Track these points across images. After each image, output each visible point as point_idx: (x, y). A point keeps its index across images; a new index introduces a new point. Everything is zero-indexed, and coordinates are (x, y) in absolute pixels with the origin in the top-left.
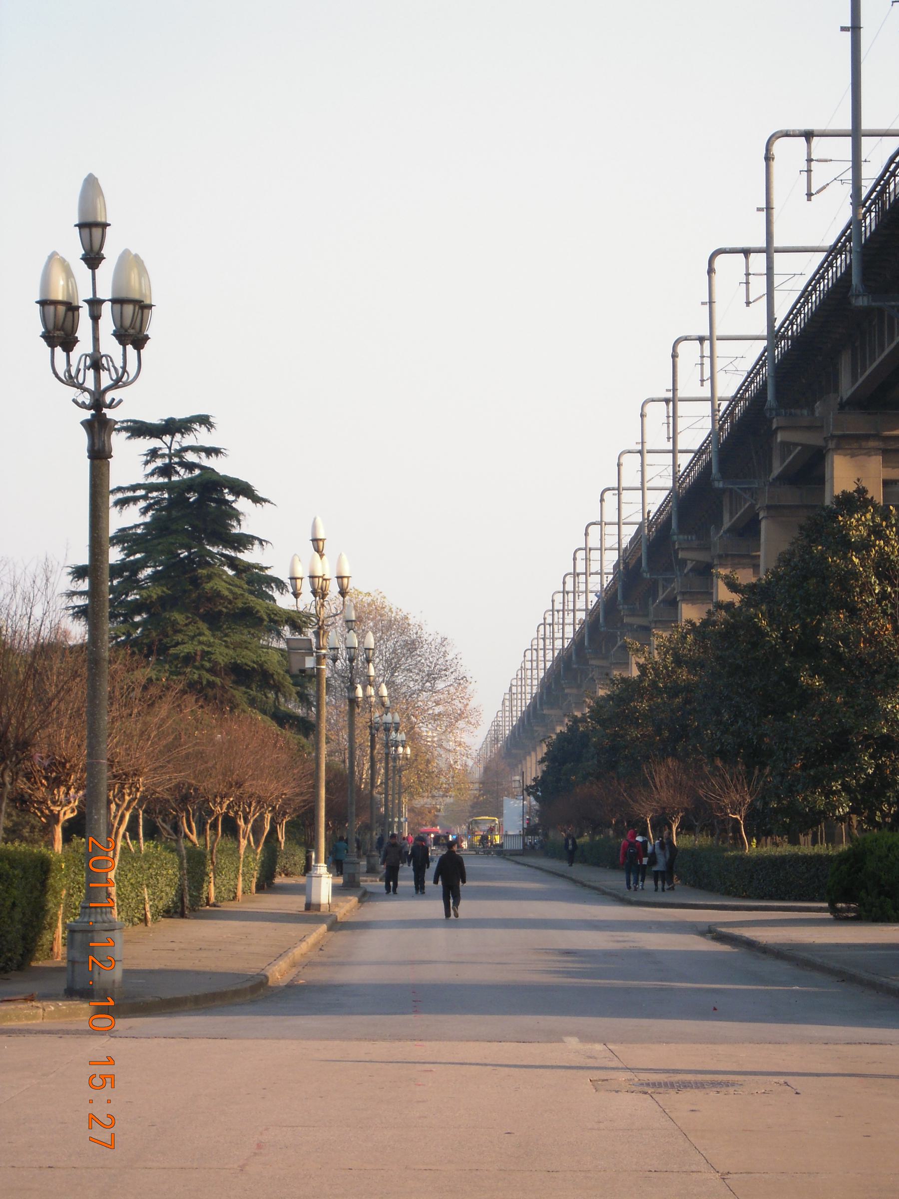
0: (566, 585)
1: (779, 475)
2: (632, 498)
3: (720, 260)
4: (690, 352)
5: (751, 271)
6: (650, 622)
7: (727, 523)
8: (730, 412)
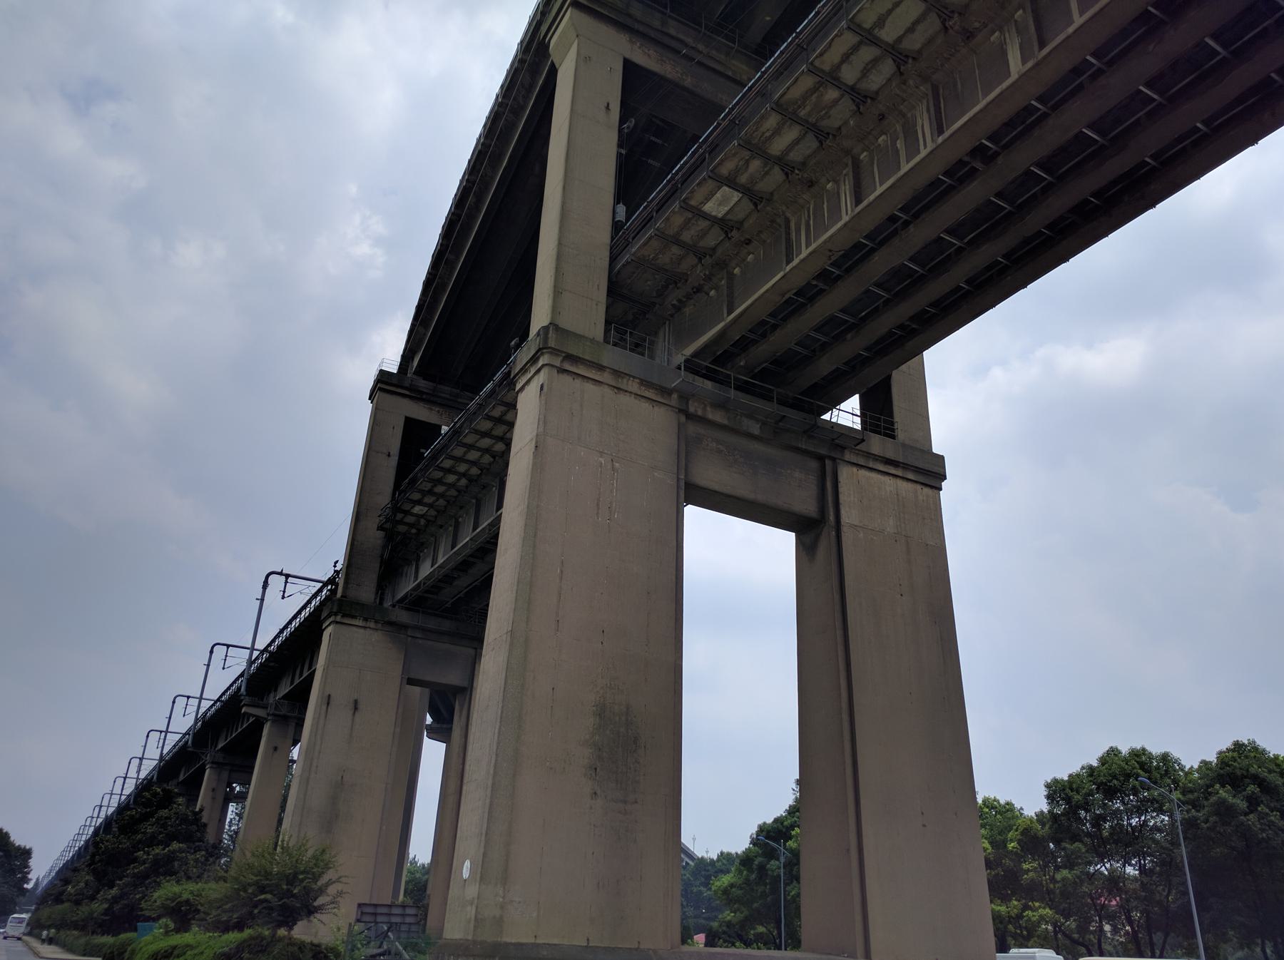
0: (213, 655)
1: (222, 747)
2: (104, 809)
3: (178, 698)
4: (154, 736)
5: (290, 579)
6: (268, 715)
7: (181, 778)
8: (142, 783)
